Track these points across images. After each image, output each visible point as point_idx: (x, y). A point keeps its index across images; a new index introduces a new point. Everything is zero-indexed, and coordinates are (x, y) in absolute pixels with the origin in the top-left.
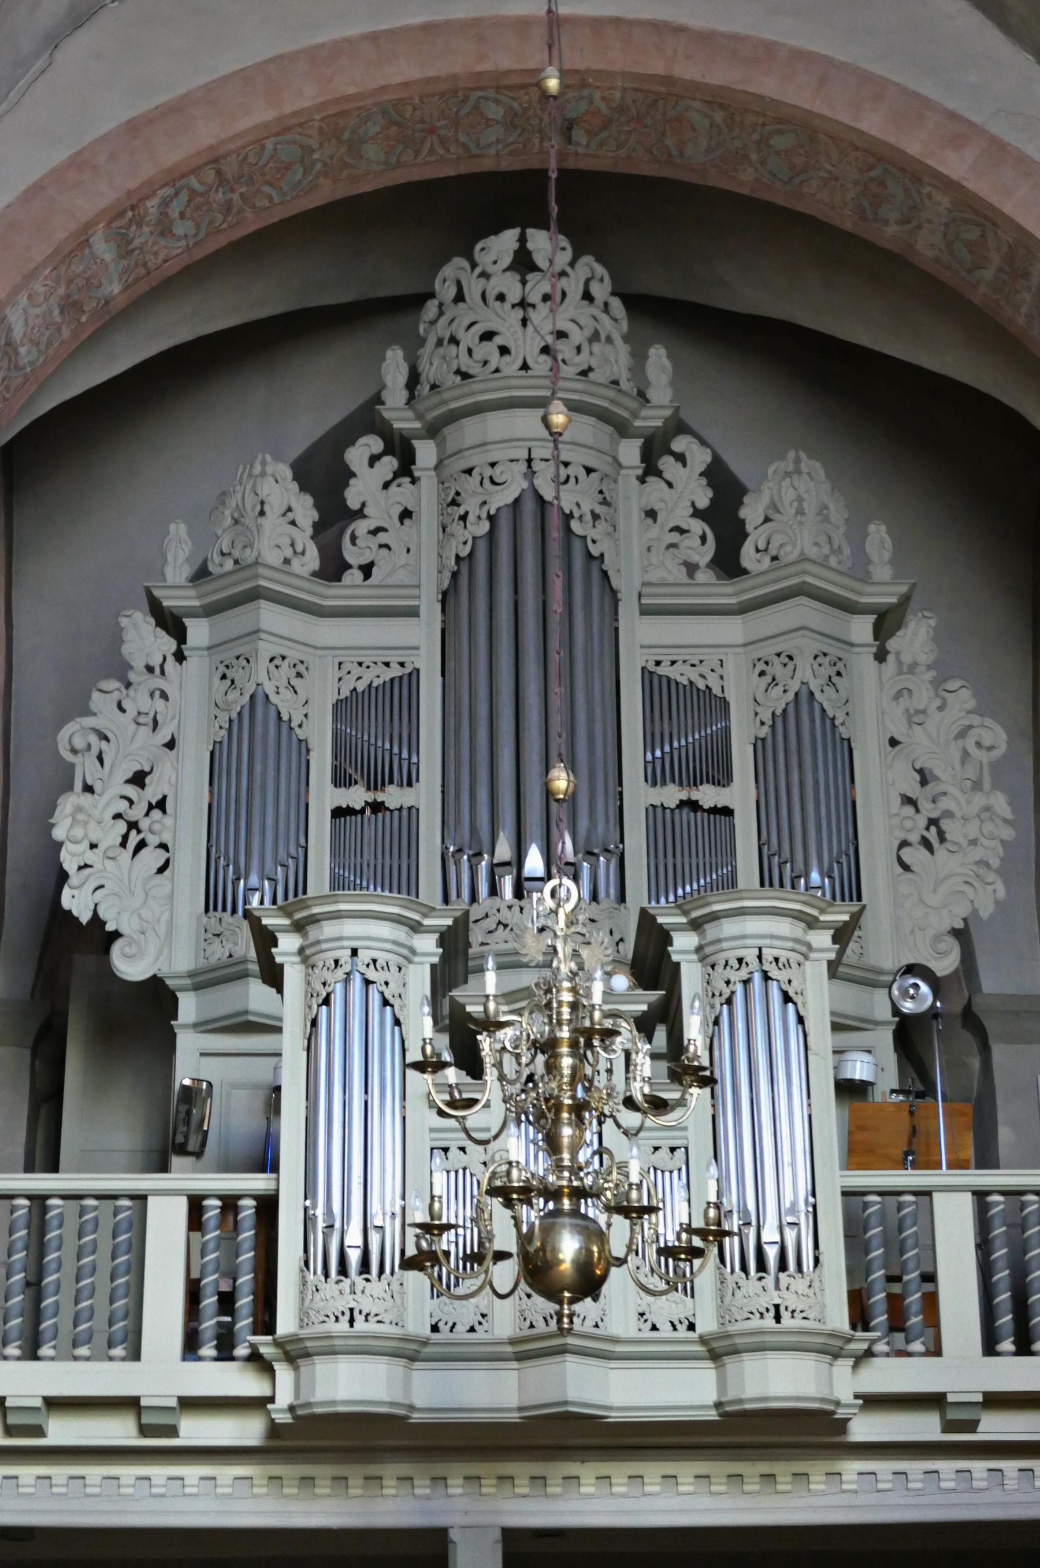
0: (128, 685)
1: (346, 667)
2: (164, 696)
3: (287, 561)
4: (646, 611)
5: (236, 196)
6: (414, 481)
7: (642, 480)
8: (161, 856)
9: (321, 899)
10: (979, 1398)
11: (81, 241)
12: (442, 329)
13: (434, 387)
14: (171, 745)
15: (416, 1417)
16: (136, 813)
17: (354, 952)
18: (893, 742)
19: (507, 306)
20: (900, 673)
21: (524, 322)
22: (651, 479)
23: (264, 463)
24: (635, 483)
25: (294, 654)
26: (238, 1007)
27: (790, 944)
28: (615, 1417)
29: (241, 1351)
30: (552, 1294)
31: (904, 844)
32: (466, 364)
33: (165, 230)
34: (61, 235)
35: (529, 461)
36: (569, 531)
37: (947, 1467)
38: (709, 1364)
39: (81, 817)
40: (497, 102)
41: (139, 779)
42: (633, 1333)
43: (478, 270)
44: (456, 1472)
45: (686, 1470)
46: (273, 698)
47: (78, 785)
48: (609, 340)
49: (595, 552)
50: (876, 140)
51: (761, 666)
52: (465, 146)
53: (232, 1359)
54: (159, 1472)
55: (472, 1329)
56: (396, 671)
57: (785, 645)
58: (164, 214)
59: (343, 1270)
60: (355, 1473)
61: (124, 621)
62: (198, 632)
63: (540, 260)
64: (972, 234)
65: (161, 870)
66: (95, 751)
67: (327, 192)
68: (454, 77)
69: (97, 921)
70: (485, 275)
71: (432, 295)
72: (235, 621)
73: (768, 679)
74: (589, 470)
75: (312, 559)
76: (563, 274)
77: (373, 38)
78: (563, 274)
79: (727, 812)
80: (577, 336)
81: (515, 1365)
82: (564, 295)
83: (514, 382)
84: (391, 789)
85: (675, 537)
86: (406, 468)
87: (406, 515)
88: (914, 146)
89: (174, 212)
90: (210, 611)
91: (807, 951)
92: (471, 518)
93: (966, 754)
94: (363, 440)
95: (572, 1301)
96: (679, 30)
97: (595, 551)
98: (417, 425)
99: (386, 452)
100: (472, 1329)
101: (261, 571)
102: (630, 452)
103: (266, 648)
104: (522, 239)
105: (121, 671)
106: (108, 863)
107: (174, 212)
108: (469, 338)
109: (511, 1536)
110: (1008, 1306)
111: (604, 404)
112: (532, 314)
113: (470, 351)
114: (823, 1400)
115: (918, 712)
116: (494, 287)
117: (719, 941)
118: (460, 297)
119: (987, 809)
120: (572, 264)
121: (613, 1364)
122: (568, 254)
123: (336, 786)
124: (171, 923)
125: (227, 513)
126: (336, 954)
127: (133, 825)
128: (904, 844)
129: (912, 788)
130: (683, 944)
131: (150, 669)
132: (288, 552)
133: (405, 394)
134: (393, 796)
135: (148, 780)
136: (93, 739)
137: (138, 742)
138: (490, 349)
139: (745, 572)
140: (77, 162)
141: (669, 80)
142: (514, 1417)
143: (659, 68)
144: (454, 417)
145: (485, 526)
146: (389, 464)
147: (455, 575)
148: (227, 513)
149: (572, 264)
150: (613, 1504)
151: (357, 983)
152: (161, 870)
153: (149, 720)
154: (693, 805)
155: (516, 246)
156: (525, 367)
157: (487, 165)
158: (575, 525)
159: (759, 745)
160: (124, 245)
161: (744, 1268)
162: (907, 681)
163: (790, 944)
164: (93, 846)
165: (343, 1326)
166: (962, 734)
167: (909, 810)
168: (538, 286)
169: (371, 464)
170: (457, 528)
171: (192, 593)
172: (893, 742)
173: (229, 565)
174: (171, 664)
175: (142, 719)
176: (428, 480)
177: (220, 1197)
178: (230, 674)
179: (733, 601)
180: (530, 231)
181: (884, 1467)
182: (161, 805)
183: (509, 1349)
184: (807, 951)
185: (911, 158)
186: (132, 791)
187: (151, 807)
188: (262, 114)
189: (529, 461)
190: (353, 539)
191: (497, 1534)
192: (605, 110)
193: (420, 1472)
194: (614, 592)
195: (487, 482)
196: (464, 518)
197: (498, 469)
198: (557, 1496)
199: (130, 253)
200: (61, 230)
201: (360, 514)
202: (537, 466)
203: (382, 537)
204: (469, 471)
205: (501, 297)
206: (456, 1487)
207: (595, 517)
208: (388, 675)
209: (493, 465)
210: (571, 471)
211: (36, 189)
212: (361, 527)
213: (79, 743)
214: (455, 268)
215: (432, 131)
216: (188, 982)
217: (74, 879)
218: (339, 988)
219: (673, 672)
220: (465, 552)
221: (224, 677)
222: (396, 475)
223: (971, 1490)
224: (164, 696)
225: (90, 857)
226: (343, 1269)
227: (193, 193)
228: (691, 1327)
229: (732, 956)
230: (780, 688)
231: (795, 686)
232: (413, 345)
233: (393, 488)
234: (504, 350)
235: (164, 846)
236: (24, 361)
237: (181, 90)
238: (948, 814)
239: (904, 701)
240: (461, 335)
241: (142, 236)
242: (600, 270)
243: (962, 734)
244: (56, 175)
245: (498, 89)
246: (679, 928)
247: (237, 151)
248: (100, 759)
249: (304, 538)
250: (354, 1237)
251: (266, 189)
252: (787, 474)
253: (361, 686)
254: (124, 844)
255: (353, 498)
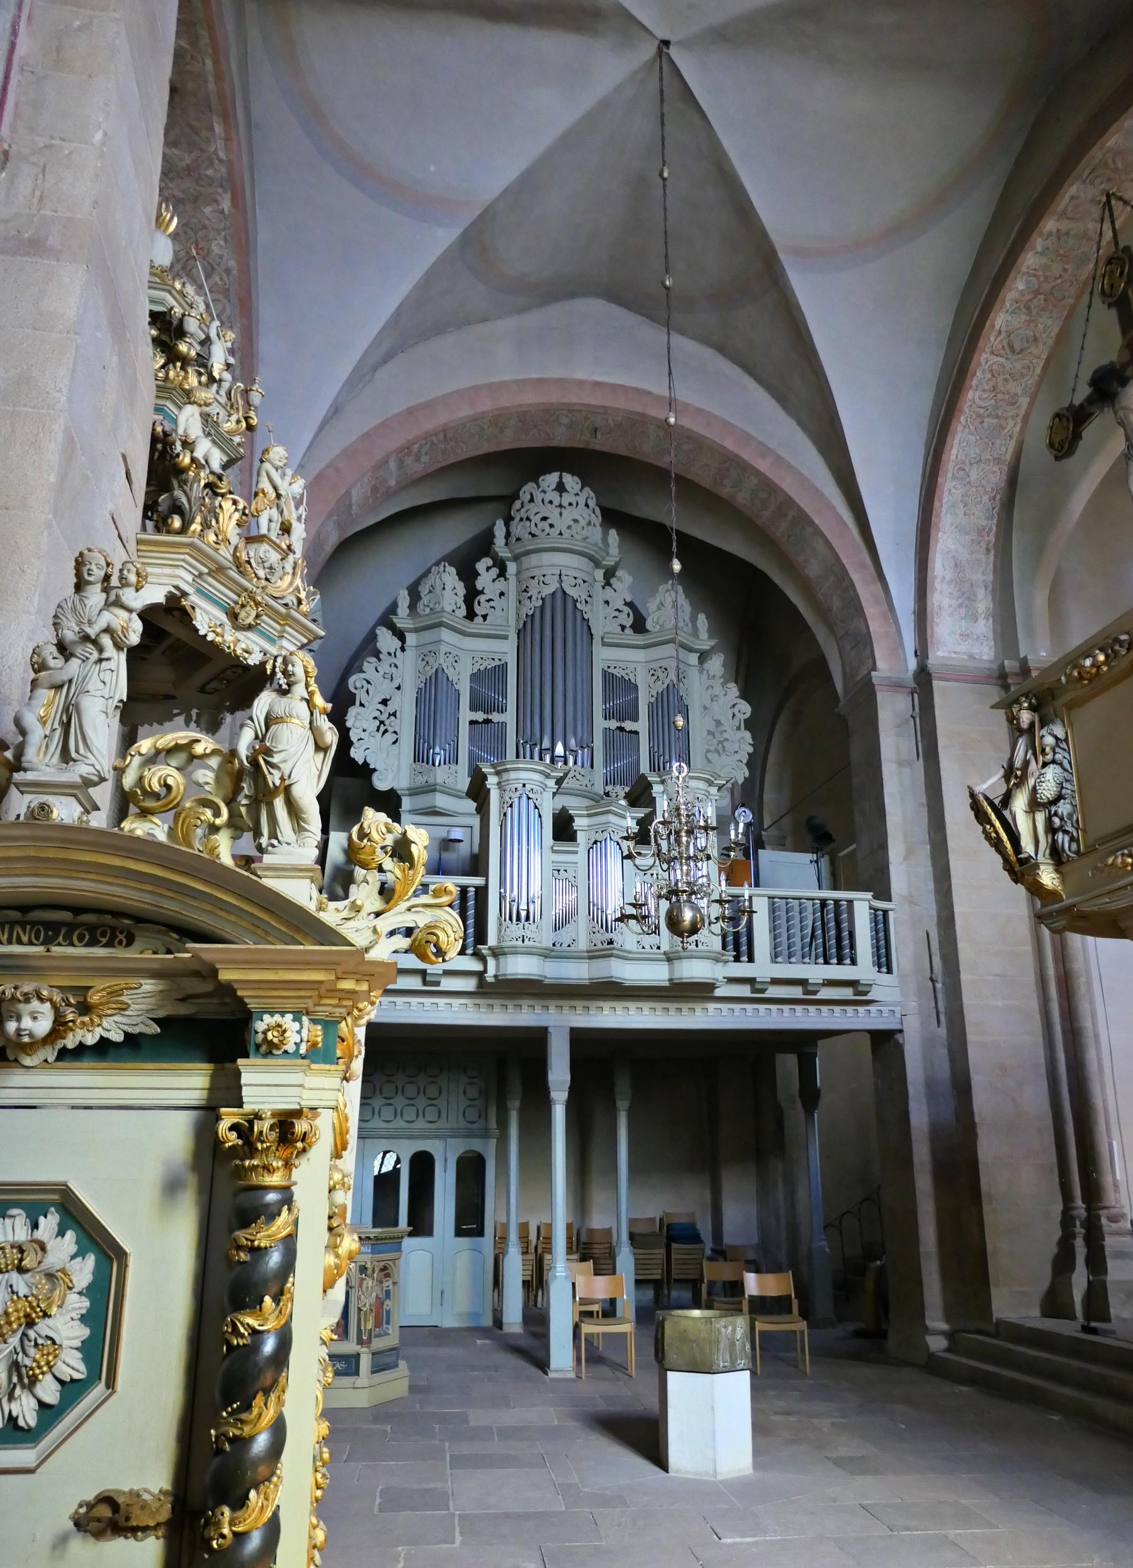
0: (380, 660)
1: (475, 660)
2: (396, 666)
3: (454, 611)
4: (604, 644)
5: (449, 447)
6: (506, 579)
7: (603, 587)
8: (394, 737)
9: (512, 762)
10: (769, 980)
11: (385, 462)
12: (523, 513)
13: (518, 539)
14: (398, 688)
15: (547, 981)
16: (384, 717)
17: (524, 785)
18: (705, 708)
19: (554, 506)
20: (708, 678)
21: (561, 514)
22: (607, 587)
23: (444, 566)
24: (601, 588)
25: (455, 652)
26: (430, 805)
27: (703, 792)
28: (628, 983)
29: (470, 951)
30: (681, 935)
31: (708, 751)
32: (534, 530)
33: (418, 459)
34: (378, 458)
35: (560, 575)
36: (576, 606)
37: (749, 1007)
38: (666, 963)
39: (359, 717)
40: (567, 416)
41: (384, 702)
42: (635, 950)
43: (541, 489)
44: (552, 1005)
45: (646, 1006)
46: (446, 670)
47: (357, 703)
48: (594, 525)
49: (586, 617)
50: (731, 452)
51: (652, 672)
52: (548, 435)
53: (465, 955)
54: (428, 1001)
55: (569, 946)
56: (497, 663)
57: (664, 664)
58: (419, 452)
59: (518, 919)
60: (510, 1004)
61: (378, 632)
62: (411, 639)
63: (568, 487)
64: (763, 495)
65: (394, 743)
66: (365, 689)
67: (486, 448)
68: (552, 404)
69: (366, 764)
70: (544, 492)
71: (518, 498)
72: (429, 636)
73: (655, 678)
74: (584, 582)
75: (463, 611)
76: (577, 494)
77: (517, 382)
78: (577, 494)
79: (636, 733)
80: (583, 522)
81: (587, 961)
82: (577, 504)
83: (555, 540)
84: (495, 714)
85: (617, 614)
86: (502, 573)
87: (502, 594)
88: (746, 455)
89: (423, 451)
90: (417, 630)
91: (708, 794)
92: (533, 598)
93: (734, 715)
94: (484, 560)
95: (687, 937)
96: (649, 393)
97: (586, 617)
98: (510, 555)
99: (494, 566)
100: (569, 946)
101: (445, 614)
102: (599, 574)
103: (444, 648)
104: (561, 477)
105: (377, 654)
106: (371, 738)
107: (423, 451)
108: (536, 519)
109: (573, 1030)
110: (732, 942)
111: (593, 553)
112: (563, 510)
113: (536, 525)
114: (540, 975)
115: (716, 696)
116: (548, 498)
117: (508, 780)
118: (532, 500)
119: (743, 738)
120: (581, 490)
121: (627, 962)
122: (579, 486)
123: (606, 719)
124: (399, 767)
125: (427, 587)
126: (516, 786)
127: (382, 722)
128: (708, 751)
129: (712, 728)
130: (492, 781)
131: (389, 654)
132: (455, 608)
133: (504, 541)
134: (495, 717)
135: (389, 703)
136: (365, 683)
137: (384, 686)
138: (545, 525)
139: (647, 631)
140: (385, 425)
141: (643, 415)
142: (587, 982)
143: (639, 409)
144: (527, 553)
145: (540, 602)
146: (495, 571)
147: (525, 623)
148: (427, 587)
149: (581, 490)
150: (642, 1018)
151: (525, 797)
152: (394, 743)
153: (389, 676)
154: (621, 729)
155: (558, 480)
156: (561, 534)
157: (554, 443)
158: (578, 605)
159: (650, 705)
160: (401, 464)
161: (511, 919)
162: (711, 682)
163: (703, 792)
164: (364, 731)
165: (520, 942)
166: (734, 706)
167: (710, 737)
168: (567, 499)
169: (487, 571)
170: (527, 602)
171: (411, 621)
172: (705, 708)
173: (428, 610)
174: (399, 652)
175: (386, 676)
176: (512, 580)
177: (475, 887)
178: (426, 659)
179: (412, 626)
180: (564, 474)
181: (724, 1006)
182: (394, 714)
183: (586, 954)
184: (544, 788)
185: (744, 461)
186: (381, 707)
187: (390, 715)
188: (466, 412)
189: (560, 575)
190: (479, 603)
191: (568, 1030)
192: (612, 423)
193: (538, 1005)
194: (592, 635)
195: (541, 583)
196: (530, 598)
197: (546, 578)
198: (593, 1015)
199: (402, 468)
200: (378, 456)
201: (482, 592)
202: (563, 578)
203: (492, 604)
204: (533, 578)
205: (551, 502)
206: (552, 1010)
207: (587, 602)
208: (494, 664)
209: (544, 576)
210: (578, 581)
211: (366, 436)
212: (482, 598)
213: (358, 685)
214: (530, 487)
215: (536, 426)
216: (407, 792)
217: (356, 744)
218: (516, 800)
219: (615, 672)
220: (530, 613)
221: (423, 660)
222: (499, 576)
223: (758, 1016)
224: (396, 666)
225: (363, 735)
226: (518, 919)
227: (433, 443)
228: (659, 948)
229: (513, 787)
230: (661, 682)
231: (667, 682)
232: (508, 519)
233: (497, 581)
234: (551, 526)
235: (395, 732)
236: (353, 512)
237: (432, 396)
238: (727, 740)
239: (710, 691)
240: (531, 517)
241: (409, 461)
242: (592, 494)
243: (734, 706)
244: (376, 429)
245: (569, 411)
246: (656, 782)
247: (454, 427)
248: (367, 692)
249: (460, 601)
250: (523, 906)
251: (462, 445)
252: (668, 591)
253: (482, 668)
254: (378, 730)
255: (479, 585)
